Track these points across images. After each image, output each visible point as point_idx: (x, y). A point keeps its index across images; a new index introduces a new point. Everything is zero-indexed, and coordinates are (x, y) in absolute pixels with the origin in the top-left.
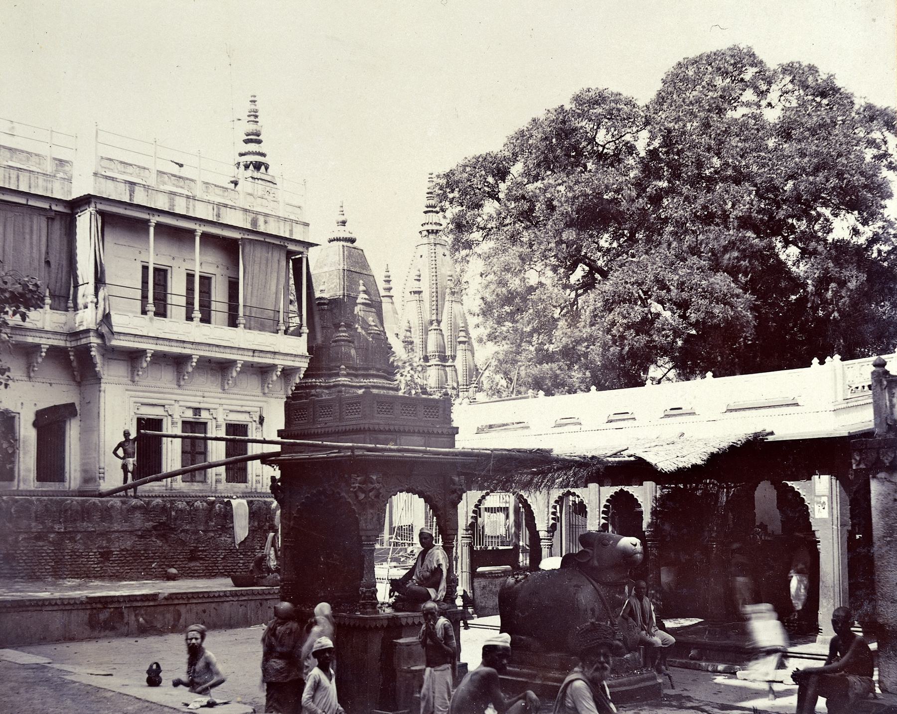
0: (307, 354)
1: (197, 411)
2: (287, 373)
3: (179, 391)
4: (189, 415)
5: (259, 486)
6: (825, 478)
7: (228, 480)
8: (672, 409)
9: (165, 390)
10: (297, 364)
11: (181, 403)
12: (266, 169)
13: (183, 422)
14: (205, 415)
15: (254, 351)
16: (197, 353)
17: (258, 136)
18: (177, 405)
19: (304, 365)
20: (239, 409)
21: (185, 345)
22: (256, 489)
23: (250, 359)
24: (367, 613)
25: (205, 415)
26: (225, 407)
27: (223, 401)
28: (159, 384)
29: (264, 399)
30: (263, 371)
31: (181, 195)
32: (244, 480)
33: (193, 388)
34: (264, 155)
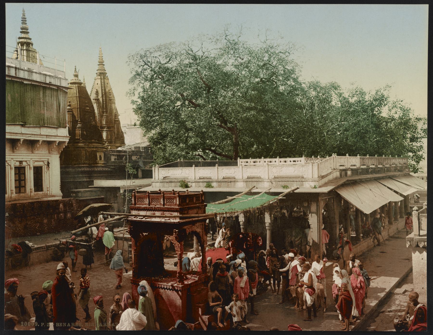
0: (68, 135)
1: (21, 162)
2: (60, 143)
3: (33, 155)
4: (18, 164)
5: (48, 192)
6: (244, 255)
7: (35, 191)
8: (340, 166)
9: (20, 155)
10: (64, 140)
11: (14, 159)
12: (32, 45)
13: (15, 167)
14: (24, 164)
15: (47, 136)
16: (22, 138)
17: (28, 30)
18: (12, 160)
19: (67, 140)
20: (39, 160)
21: (17, 135)
22: (47, 194)
23: (45, 139)
24: (185, 214)
25: (24, 164)
26: (33, 160)
27: (32, 157)
28: (20, 152)
29: (50, 155)
30: (49, 143)
31: (12, 67)
32: (42, 190)
33: (20, 152)
34: (30, 39)
